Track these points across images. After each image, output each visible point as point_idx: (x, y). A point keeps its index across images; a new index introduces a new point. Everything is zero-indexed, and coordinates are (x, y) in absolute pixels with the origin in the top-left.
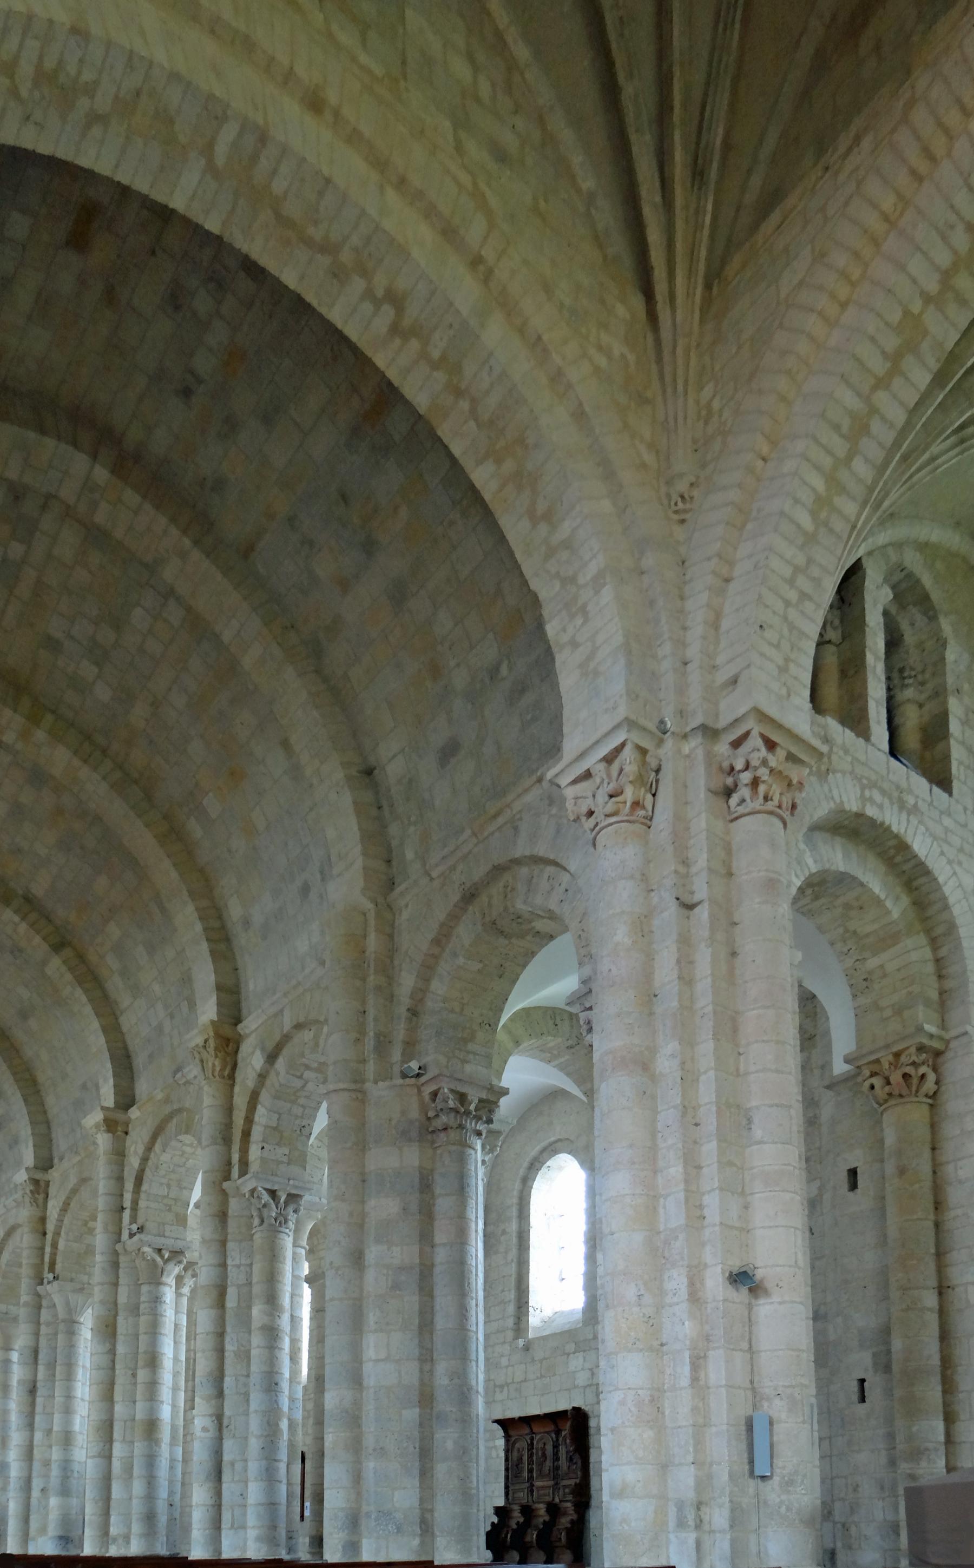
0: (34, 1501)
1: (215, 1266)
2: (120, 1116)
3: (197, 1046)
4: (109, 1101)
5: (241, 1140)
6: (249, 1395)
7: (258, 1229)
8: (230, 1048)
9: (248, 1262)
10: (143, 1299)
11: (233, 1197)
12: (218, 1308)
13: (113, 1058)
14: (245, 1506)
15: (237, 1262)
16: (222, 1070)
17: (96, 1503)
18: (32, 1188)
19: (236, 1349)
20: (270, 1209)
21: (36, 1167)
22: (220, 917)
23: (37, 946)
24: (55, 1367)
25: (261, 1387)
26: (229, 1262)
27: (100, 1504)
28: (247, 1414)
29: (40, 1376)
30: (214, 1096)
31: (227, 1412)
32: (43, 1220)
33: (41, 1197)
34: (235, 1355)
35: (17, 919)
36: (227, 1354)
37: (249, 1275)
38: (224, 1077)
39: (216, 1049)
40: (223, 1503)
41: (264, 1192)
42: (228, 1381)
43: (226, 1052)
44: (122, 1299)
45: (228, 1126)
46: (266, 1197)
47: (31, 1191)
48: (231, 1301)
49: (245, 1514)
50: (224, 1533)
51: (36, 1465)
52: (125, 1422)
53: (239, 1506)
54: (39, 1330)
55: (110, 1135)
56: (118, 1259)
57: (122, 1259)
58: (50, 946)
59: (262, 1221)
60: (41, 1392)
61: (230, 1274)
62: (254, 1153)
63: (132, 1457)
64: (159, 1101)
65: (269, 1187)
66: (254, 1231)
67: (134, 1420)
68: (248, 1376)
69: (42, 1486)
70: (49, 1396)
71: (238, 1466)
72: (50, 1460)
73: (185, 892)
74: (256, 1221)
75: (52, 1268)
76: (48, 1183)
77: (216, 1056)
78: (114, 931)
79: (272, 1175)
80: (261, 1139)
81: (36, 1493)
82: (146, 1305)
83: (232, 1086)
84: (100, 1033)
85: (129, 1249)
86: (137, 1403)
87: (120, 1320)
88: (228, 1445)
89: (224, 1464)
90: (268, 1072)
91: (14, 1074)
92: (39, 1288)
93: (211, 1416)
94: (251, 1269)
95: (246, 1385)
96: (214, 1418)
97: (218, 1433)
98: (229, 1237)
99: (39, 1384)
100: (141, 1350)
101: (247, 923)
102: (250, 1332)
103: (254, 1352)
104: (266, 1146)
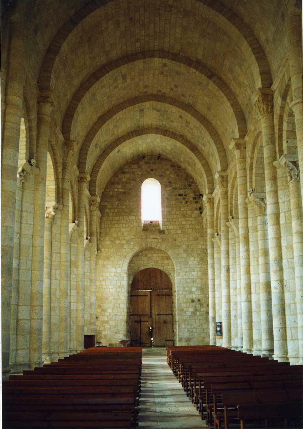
0: (232, 321)
1: (273, 204)
2: (241, 141)
3: (256, 101)
4: (237, 136)
5: (279, 140)
6: (294, 269)
7: (291, 182)
8: (269, 98)
9: (288, 199)
10: (258, 223)
11: (278, 168)
12: (276, 225)
13: (237, 116)
14: (297, 328)
15: (283, 200)
16: (267, 109)
17: (246, 324)
18: (221, 180)
19: (286, 245)
20: (295, 171)
21: (221, 171)
22: (258, 42)
23: (204, 78)
24: (236, 259)
25: (299, 263)
26: (280, 201)
27: (248, 324)
28: (294, 279)
29: (231, 263)
30: (265, 122)
31: (285, 278)
32: (226, 193)
33: (225, 183)
34: (286, 248)
35: (195, 70)
36: (283, 248)
37: (289, 205)
38: (268, 113)
39: (263, 100)
40: (287, 326)
41: (290, 163)
42: (284, 262)
43: (268, 101)
44: (250, 225)
45: (273, 134)
46: (291, 165)
47: (221, 181)
48: (282, 221)
49: (297, 332)
50: (288, 342)
51: (232, 304)
52: (256, 283)
53: (294, 328)
54: (229, 242)
55: (239, 150)
56: (247, 206)
57: (249, 206)
58: (208, 77)
59: (291, 178)
60: (231, 271)
61: (280, 207)
62: (285, 145)
63: (260, 301)
64: (253, 131)
65: (292, 160)
66: (289, 183)
67: (259, 282)
68: (293, 258)
69: (234, 315)
70: (234, 272)
71: (292, 306)
72: (237, 302)
73: (242, 37)
74: (289, 178)
75: (231, 215)
76: (227, 177)
77: (264, 104)
78: (227, 63)
79: (293, 154)
80: (286, 138)
81: (232, 318)
82: (260, 226)
83: (273, 115)
84: (231, 107)
85: (251, 201)
86: (260, 274)
87: (250, 234)
88: (287, 295)
89: (286, 305)
90: (284, 105)
91: (210, 133)
92: (227, 223)
93: (277, 281)
94: (290, 202)
95: (292, 263)
96: (279, 282)
97: (281, 290)
98: (279, 188)
99: (231, 267)
100: (260, 248)
101: (267, 40)
102: (292, 235)
103: (295, 246)
104: (289, 140)
